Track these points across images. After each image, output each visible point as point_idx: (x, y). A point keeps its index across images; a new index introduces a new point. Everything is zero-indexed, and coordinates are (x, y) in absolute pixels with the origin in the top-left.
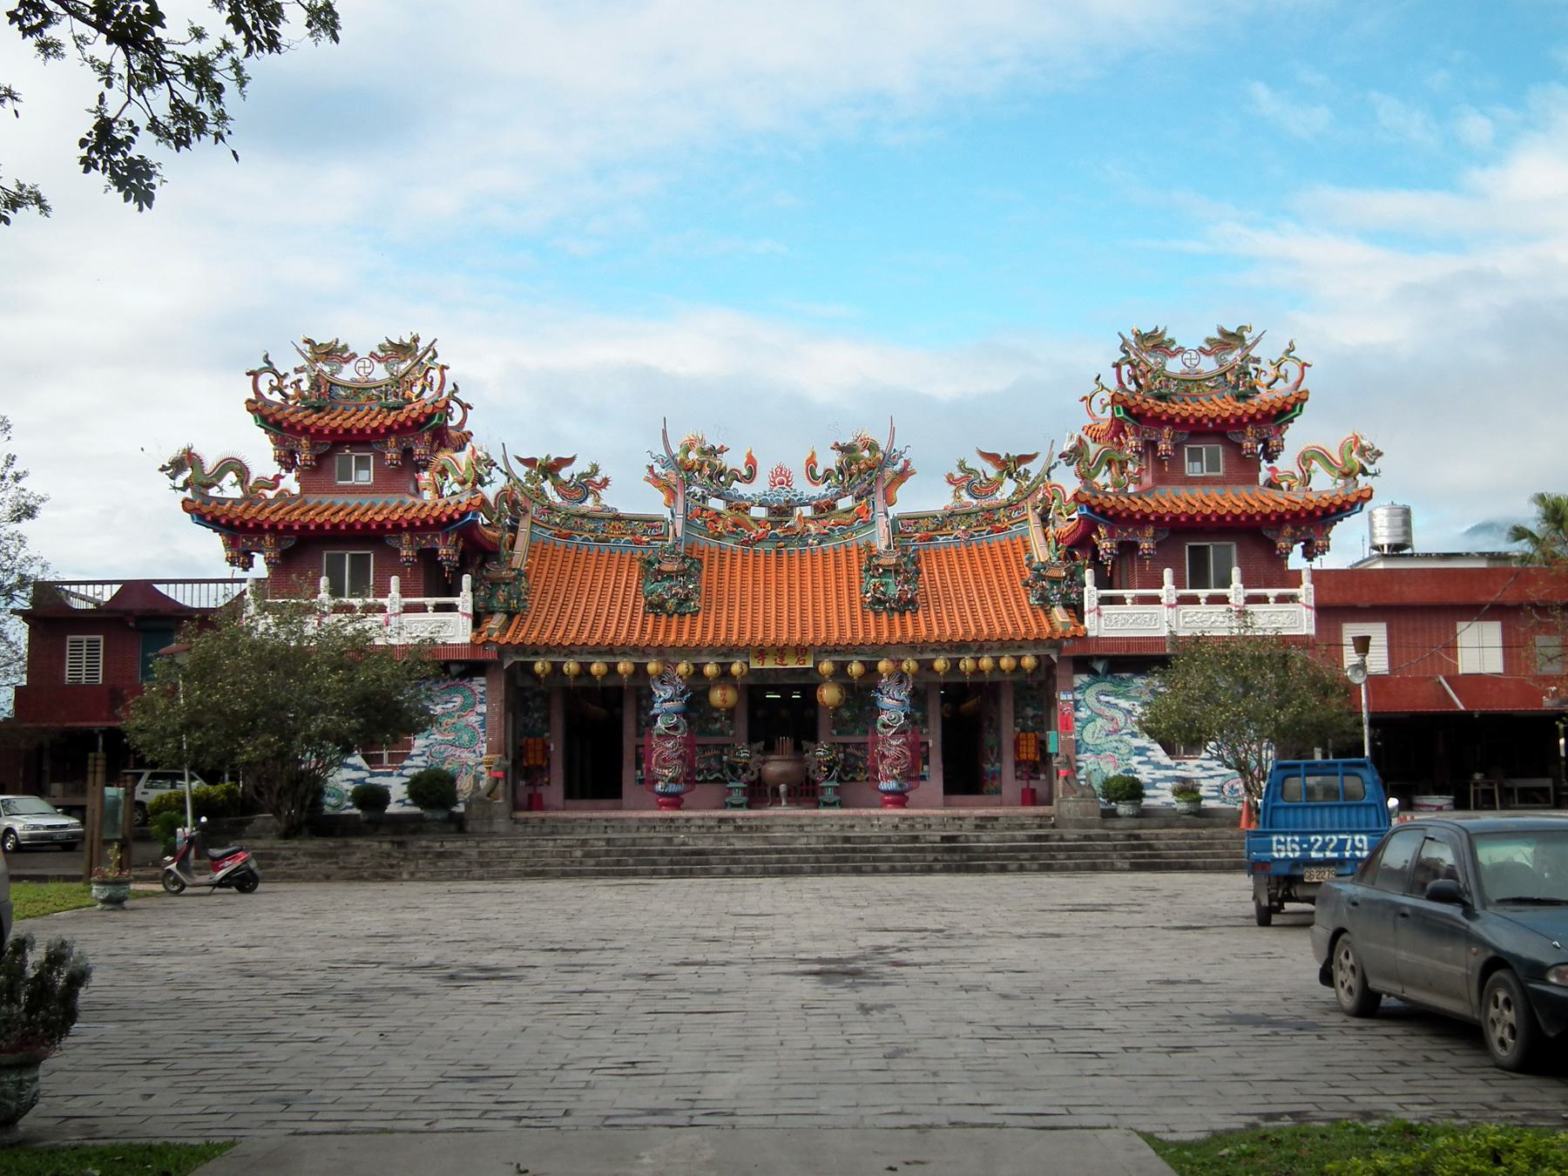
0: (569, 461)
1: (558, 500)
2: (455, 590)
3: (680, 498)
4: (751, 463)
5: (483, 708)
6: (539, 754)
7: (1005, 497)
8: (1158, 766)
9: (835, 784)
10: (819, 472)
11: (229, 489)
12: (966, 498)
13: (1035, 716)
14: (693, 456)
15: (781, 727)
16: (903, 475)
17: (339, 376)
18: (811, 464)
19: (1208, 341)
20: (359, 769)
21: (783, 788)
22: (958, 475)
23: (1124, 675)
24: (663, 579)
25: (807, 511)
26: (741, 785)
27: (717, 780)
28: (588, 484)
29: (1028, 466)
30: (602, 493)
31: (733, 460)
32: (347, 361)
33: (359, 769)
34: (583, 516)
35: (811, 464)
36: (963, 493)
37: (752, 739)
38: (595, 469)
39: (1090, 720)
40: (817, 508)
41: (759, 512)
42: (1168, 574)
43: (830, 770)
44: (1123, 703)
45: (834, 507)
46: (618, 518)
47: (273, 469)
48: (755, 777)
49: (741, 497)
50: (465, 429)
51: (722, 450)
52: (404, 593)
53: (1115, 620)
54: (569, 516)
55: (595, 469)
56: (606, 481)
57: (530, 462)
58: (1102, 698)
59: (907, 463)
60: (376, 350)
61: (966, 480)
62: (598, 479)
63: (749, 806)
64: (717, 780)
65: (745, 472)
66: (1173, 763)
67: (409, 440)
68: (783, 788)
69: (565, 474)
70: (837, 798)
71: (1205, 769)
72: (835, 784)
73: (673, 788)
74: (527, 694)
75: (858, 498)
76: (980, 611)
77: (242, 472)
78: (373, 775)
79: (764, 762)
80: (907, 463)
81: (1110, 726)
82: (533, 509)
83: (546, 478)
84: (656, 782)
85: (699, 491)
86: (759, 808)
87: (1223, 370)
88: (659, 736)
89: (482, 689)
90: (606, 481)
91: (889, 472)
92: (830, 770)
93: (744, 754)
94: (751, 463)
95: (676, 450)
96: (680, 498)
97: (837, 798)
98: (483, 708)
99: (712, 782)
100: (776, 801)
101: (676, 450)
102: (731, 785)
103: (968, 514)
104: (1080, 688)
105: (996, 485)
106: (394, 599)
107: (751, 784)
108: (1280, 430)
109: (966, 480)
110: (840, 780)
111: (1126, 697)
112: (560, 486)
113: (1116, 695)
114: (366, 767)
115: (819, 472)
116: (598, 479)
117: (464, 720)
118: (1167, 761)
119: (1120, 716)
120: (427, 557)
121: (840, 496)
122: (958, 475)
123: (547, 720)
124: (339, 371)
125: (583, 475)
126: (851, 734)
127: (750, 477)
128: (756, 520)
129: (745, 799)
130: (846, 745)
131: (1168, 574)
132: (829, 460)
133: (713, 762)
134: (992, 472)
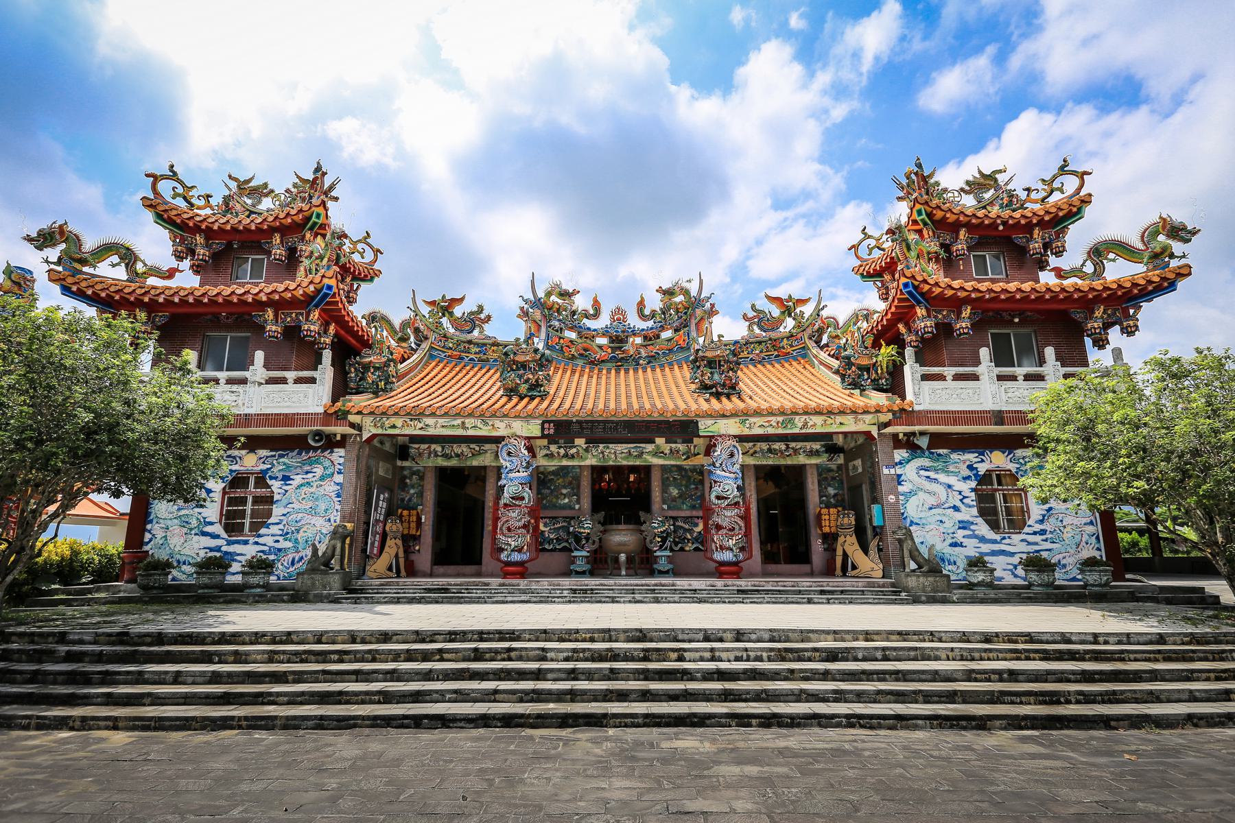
0: (461, 300)
1: (452, 331)
2: (316, 362)
3: (543, 329)
4: (596, 305)
5: (339, 478)
6: (413, 525)
7: (788, 330)
8: (983, 539)
9: (668, 553)
10: (647, 312)
11: (111, 271)
12: (757, 331)
13: (835, 495)
14: (553, 298)
15: (620, 508)
16: (712, 312)
17: (260, 207)
18: (641, 305)
19: (968, 183)
20: (218, 537)
21: (623, 557)
22: (751, 314)
23: (940, 451)
24: (518, 369)
25: (639, 340)
26: (584, 553)
27: (564, 549)
28: (476, 319)
29: (802, 309)
30: (486, 326)
31: (581, 303)
32: (266, 195)
33: (218, 537)
34: (470, 342)
35: (641, 305)
36: (755, 327)
37: (595, 509)
38: (481, 309)
39: (912, 493)
40: (645, 338)
41: (603, 341)
42: (984, 353)
43: (664, 540)
44: (942, 477)
45: (658, 337)
46: (496, 344)
47: (169, 262)
48: (596, 546)
49: (589, 329)
50: (376, 267)
51: (576, 292)
52: (267, 366)
53: (932, 394)
54: (459, 343)
55: (481, 309)
56: (489, 318)
57: (433, 303)
58: (922, 472)
59: (713, 305)
60: (291, 187)
61: (759, 319)
62: (482, 316)
63: (592, 573)
64: (564, 549)
65: (592, 312)
66: (998, 537)
67: (293, 239)
68: (623, 557)
69: (458, 311)
70: (671, 566)
71: (1029, 543)
72: (668, 553)
73: (516, 557)
74: (406, 473)
75: (676, 330)
76: (804, 395)
77: (129, 257)
78: (229, 543)
79: (604, 532)
80: (713, 305)
81: (932, 501)
82: (432, 337)
83: (444, 315)
84: (502, 550)
85: (557, 323)
86: (605, 576)
87: (982, 205)
88: (506, 505)
89: (342, 460)
90: (489, 318)
91: (699, 312)
92: (664, 540)
93: (588, 524)
94: (596, 305)
95: (541, 294)
96: (543, 329)
97: (671, 566)
98: (339, 478)
99: (560, 550)
100: (615, 573)
101: (541, 294)
102: (576, 553)
103: (760, 343)
104: (900, 463)
105: (780, 322)
106: (258, 368)
107: (595, 552)
108: (1064, 230)
109: (759, 319)
110: (672, 550)
111: (948, 473)
112: (455, 323)
113: (936, 471)
114: (224, 535)
115: (647, 312)
116: (482, 316)
117: (321, 490)
118: (991, 535)
119: (941, 491)
120: (292, 333)
121: (663, 328)
122: (751, 314)
123: (421, 494)
124: (260, 202)
125: (472, 313)
126: (680, 509)
127: (596, 315)
128: (600, 347)
129: (588, 567)
130: (675, 519)
131: (984, 353)
132: (655, 303)
133: (563, 534)
134: (776, 312)
